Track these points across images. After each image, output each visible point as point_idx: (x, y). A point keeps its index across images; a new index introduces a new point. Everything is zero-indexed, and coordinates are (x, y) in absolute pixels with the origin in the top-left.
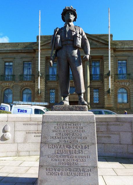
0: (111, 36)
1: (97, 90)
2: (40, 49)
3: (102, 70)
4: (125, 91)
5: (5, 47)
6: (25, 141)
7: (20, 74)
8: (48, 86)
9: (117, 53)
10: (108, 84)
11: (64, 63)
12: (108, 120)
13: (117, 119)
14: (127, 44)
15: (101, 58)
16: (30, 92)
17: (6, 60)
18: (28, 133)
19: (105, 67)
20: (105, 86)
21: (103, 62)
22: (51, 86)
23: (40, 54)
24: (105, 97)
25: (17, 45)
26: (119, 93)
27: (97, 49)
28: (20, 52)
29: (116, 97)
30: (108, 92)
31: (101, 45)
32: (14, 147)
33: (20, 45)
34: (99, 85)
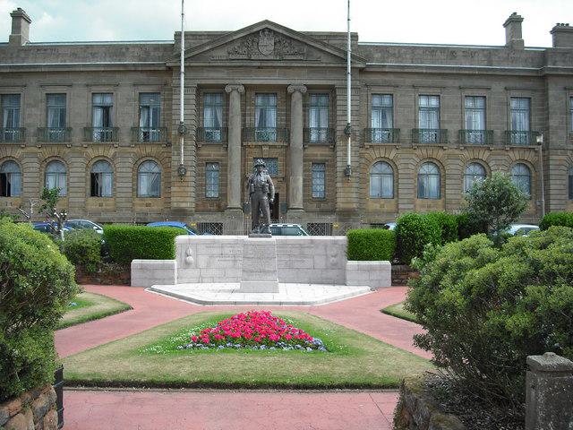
0: (355, 36)
1: (321, 168)
2: (185, 67)
3: (333, 118)
4: (389, 170)
5: (94, 55)
6: (208, 266)
7: (131, 124)
8: (202, 155)
9: (369, 76)
10: (346, 155)
11: (256, 204)
12: (302, 243)
13: (312, 241)
14: (394, 54)
15: (332, 89)
16: (156, 170)
17: (95, 89)
18: (212, 256)
19: (338, 113)
20: (338, 159)
21: (334, 100)
22: (209, 155)
23: (185, 79)
24: (339, 185)
25: (124, 50)
26: (371, 174)
27: (218, 378)
28: (133, 69)
29: (364, 181)
30: (346, 173)
31: (330, 60)
32: (196, 273)
33: (131, 50)
34: (326, 155)
